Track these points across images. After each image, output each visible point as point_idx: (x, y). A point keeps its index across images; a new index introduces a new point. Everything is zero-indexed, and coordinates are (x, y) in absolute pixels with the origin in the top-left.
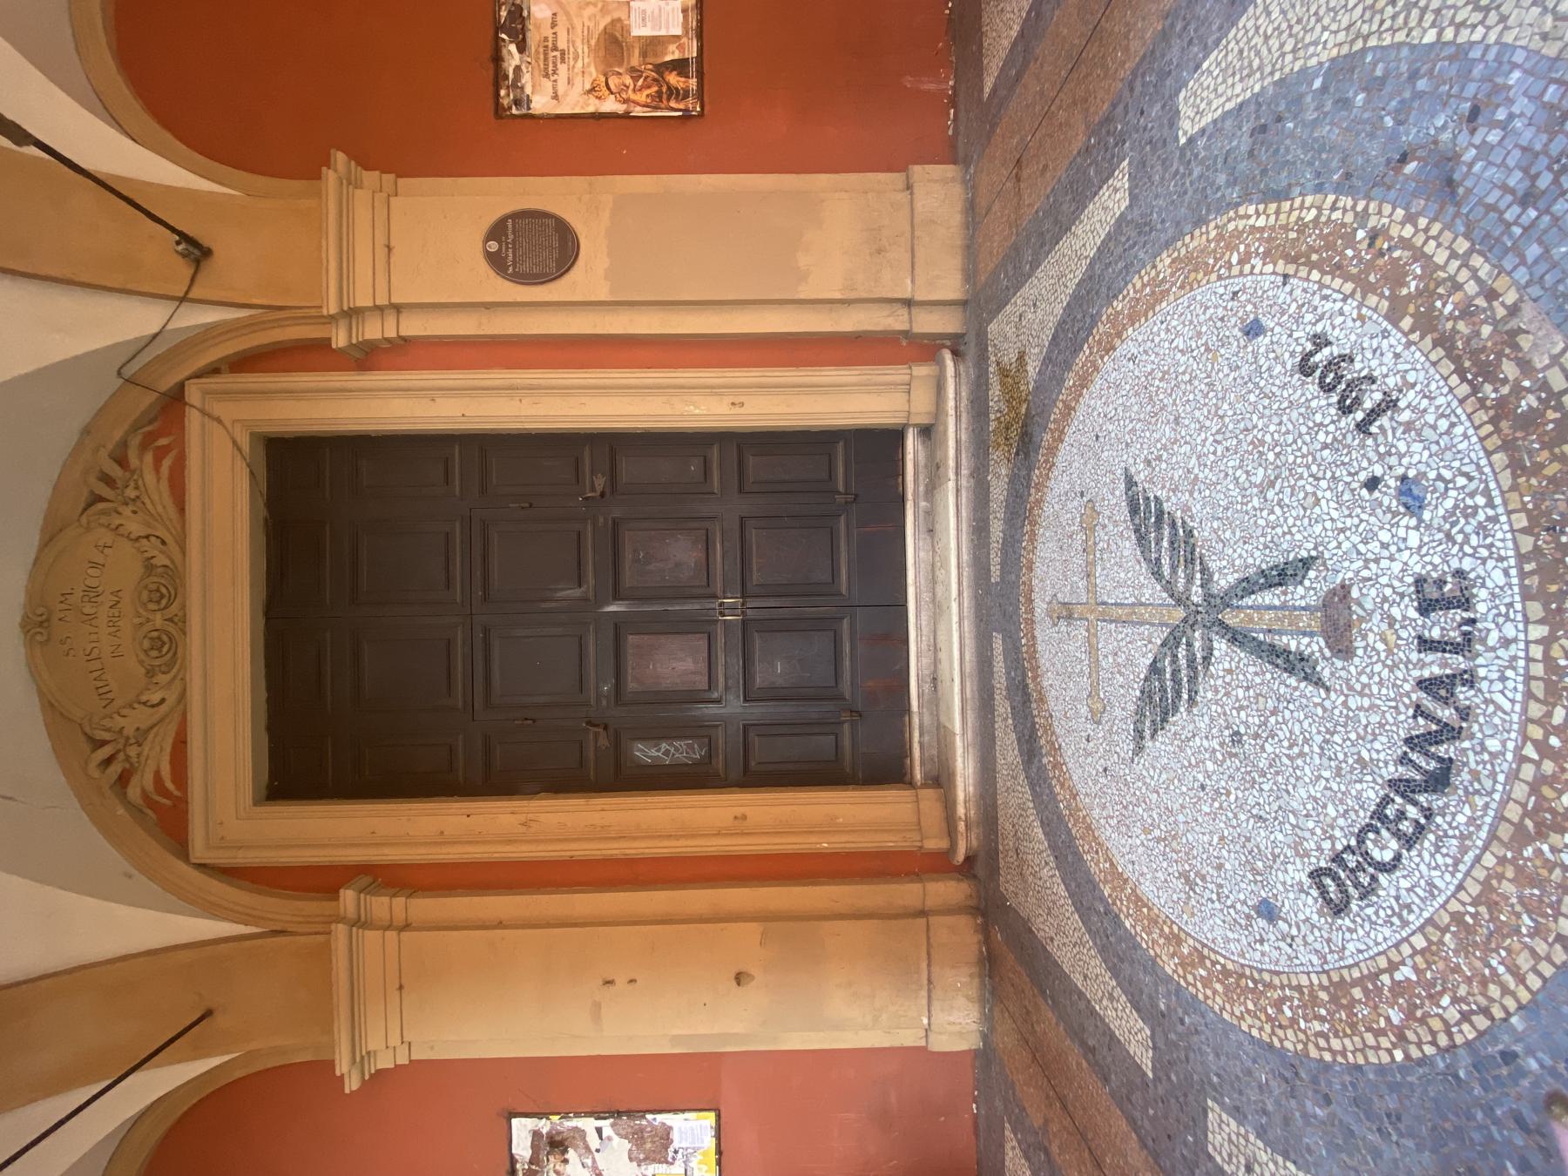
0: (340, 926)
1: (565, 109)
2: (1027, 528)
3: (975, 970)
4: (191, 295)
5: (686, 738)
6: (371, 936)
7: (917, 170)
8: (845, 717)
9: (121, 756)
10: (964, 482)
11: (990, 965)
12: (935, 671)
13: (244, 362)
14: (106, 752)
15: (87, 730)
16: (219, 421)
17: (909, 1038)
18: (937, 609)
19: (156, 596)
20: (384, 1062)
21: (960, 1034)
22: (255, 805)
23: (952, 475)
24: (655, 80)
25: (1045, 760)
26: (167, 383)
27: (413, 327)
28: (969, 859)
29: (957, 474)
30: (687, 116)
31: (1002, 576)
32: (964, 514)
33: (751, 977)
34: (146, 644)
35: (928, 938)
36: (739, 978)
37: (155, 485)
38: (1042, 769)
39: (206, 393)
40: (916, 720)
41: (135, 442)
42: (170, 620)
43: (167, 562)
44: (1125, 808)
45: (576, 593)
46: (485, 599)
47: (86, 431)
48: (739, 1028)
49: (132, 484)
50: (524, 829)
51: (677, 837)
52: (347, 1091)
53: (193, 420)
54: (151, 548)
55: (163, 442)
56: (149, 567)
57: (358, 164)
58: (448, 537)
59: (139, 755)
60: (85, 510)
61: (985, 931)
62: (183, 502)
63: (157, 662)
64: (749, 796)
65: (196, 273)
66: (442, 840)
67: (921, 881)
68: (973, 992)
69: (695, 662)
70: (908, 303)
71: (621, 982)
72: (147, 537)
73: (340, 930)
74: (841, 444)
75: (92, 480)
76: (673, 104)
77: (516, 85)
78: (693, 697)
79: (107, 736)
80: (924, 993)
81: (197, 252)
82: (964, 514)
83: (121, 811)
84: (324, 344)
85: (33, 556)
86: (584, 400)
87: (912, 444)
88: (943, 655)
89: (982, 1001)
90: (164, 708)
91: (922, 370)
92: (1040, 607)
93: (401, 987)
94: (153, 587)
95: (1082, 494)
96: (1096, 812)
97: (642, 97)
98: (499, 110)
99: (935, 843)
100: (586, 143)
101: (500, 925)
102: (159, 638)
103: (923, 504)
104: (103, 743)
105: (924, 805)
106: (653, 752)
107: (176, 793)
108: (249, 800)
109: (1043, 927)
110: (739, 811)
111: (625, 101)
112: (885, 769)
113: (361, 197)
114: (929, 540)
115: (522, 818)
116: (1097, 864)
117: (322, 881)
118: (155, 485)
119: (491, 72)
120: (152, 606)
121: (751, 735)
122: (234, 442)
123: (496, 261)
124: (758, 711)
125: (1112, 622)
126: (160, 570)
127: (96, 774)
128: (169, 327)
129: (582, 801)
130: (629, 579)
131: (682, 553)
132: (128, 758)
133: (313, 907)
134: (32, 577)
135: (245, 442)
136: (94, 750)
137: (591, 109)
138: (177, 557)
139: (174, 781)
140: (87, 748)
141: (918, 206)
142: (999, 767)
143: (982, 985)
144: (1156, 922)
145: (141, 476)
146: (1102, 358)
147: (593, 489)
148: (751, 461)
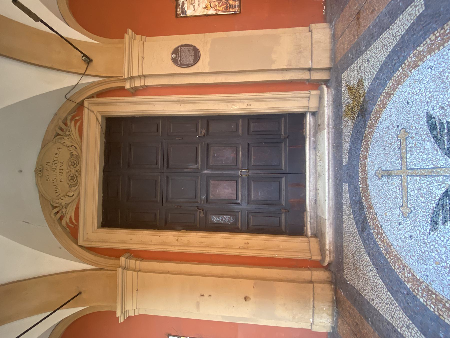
0: (120, 269)
1: (197, 14)
2: (364, 143)
3: (331, 304)
4: (86, 73)
5: (229, 215)
6: (129, 273)
7: (313, 25)
8: (283, 211)
9: (61, 211)
10: (330, 130)
11: (337, 303)
12: (316, 197)
13: (100, 94)
14: (56, 210)
15: (52, 203)
16: (93, 112)
17: (305, 325)
18: (317, 176)
19: (73, 164)
20: (131, 314)
21: (324, 326)
22: (98, 228)
23: (326, 127)
24: (225, 3)
25: (372, 231)
26: (78, 101)
27: (149, 82)
28: (329, 264)
29: (328, 127)
30: (235, 14)
31: (349, 163)
32: (330, 141)
33: (250, 299)
34: (70, 178)
35: (313, 291)
36: (246, 299)
37: (74, 132)
38: (369, 234)
39: (89, 103)
40: (309, 214)
41: (70, 117)
42: (77, 171)
43: (77, 154)
44: (424, 253)
45: (195, 167)
46: (168, 167)
47: (56, 114)
48: (246, 316)
49: (68, 130)
50: (177, 242)
51: (226, 248)
52: (120, 322)
53: (86, 111)
54: (72, 149)
55: (77, 118)
56: (72, 155)
57: (135, 33)
58: (157, 148)
59: (66, 211)
60: (55, 137)
61: (336, 292)
62: (82, 136)
63: (73, 183)
64: (260, 237)
65: (87, 67)
66: (151, 243)
67: (310, 270)
68: (330, 312)
69: (232, 190)
70: (310, 70)
71: (206, 296)
72: (71, 146)
73: (120, 270)
74: (283, 118)
75: (57, 129)
76: (231, 10)
77: (182, 8)
78: (230, 202)
79: (57, 205)
80: (311, 310)
81: (88, 60)
82: (330, 141)
83: (59, 228)
84: (123, 88)
85: (39, 151)
86: (200, 104)
87: (309, 119)
88: (320, 192)
89: (333, 316)
90: (74, 197)
91: (314, 92)
92: (370, 172)
93: (137, 290)
94: (72, 161)
95: (398, 126)
96: (404, 254)
97: (221, 8)
98: (177, 16)
99: (316, 257)
100: (204, 23)
101: (168, 273)
102: (73, 176)
103: (312, 139)
104: (56, 207)
105: (312, 244)
106: (218, 219)
107: (76, 223)
108: (96, 226)
109: (368, 294)
110: (246, 241)
111: (216, 10)
112: (297, 230)
113: (136, 42)
114: (314, 151)
115: (176, 238)
116: (404, 274)
117: (116, 254)
118: (74, 132)
119: (175, 4)
120: (72, 167)
121: (250, 216)
122: (97, 119)
123: (175, 61)
124: (253, 207)
125: (417, 176)
126: (75, 156)
127: (53, 217)
128: (80, 83)
129: (195, 234)
130: (211, 162)
131: (228, 155)
132: (62, 212)
133: (112, 262)
134: (39, 156)
135: (100, 119)
136: (53, 209)
137: (205, 13)
138: (79, 151)
139: (75, 220)
140: (51, 208)
141: (314, 37)
142: (344, 232)
143: (333, 310)
144: (441, 302)
145: (71, 128)
146: (410, 71)
147: (201, 133)
148: (252, 125)
